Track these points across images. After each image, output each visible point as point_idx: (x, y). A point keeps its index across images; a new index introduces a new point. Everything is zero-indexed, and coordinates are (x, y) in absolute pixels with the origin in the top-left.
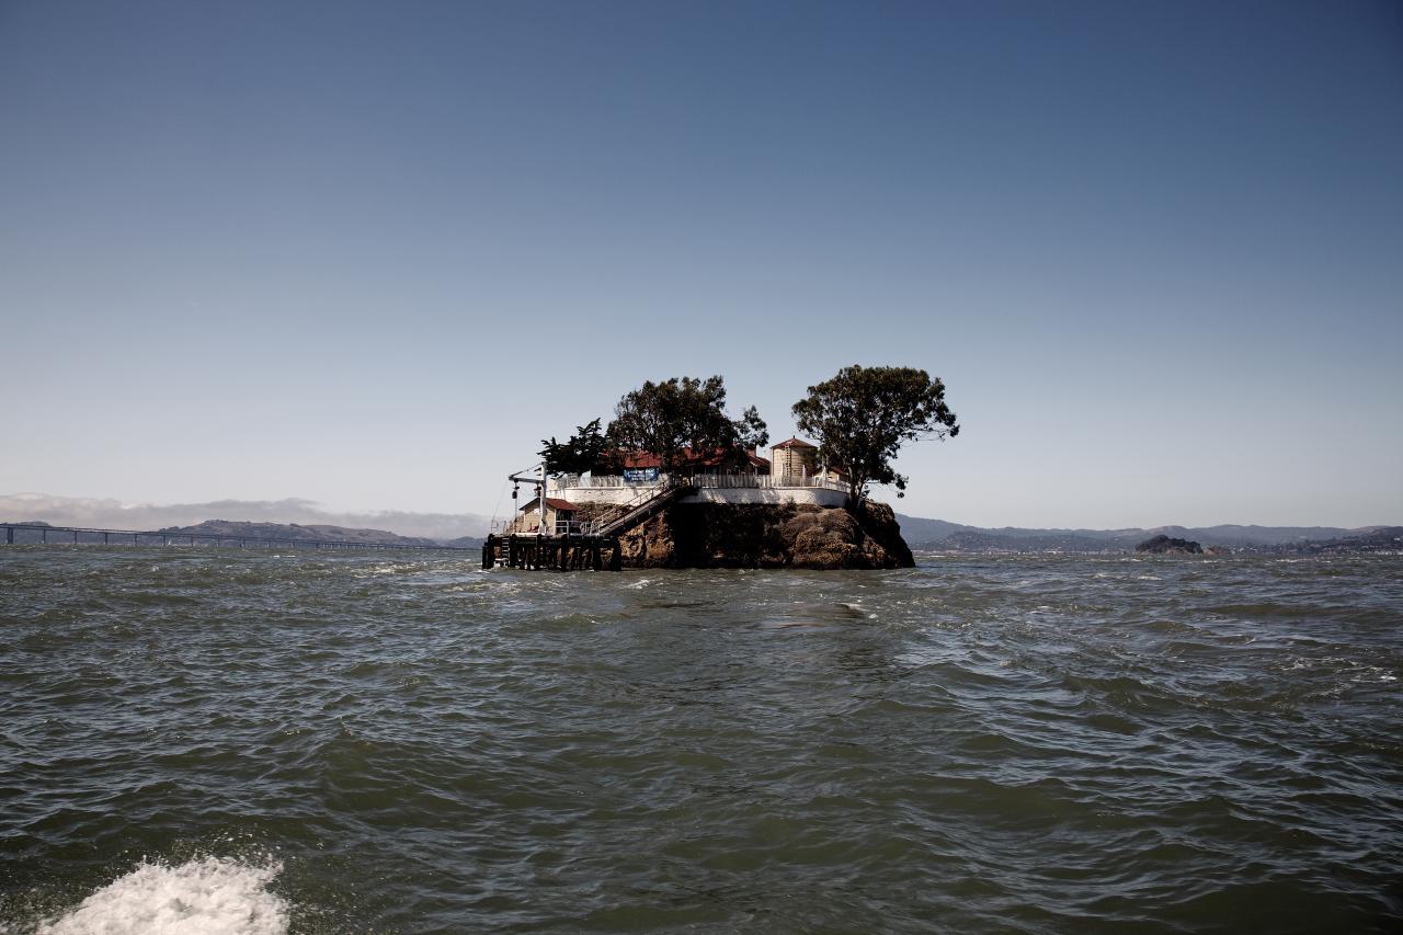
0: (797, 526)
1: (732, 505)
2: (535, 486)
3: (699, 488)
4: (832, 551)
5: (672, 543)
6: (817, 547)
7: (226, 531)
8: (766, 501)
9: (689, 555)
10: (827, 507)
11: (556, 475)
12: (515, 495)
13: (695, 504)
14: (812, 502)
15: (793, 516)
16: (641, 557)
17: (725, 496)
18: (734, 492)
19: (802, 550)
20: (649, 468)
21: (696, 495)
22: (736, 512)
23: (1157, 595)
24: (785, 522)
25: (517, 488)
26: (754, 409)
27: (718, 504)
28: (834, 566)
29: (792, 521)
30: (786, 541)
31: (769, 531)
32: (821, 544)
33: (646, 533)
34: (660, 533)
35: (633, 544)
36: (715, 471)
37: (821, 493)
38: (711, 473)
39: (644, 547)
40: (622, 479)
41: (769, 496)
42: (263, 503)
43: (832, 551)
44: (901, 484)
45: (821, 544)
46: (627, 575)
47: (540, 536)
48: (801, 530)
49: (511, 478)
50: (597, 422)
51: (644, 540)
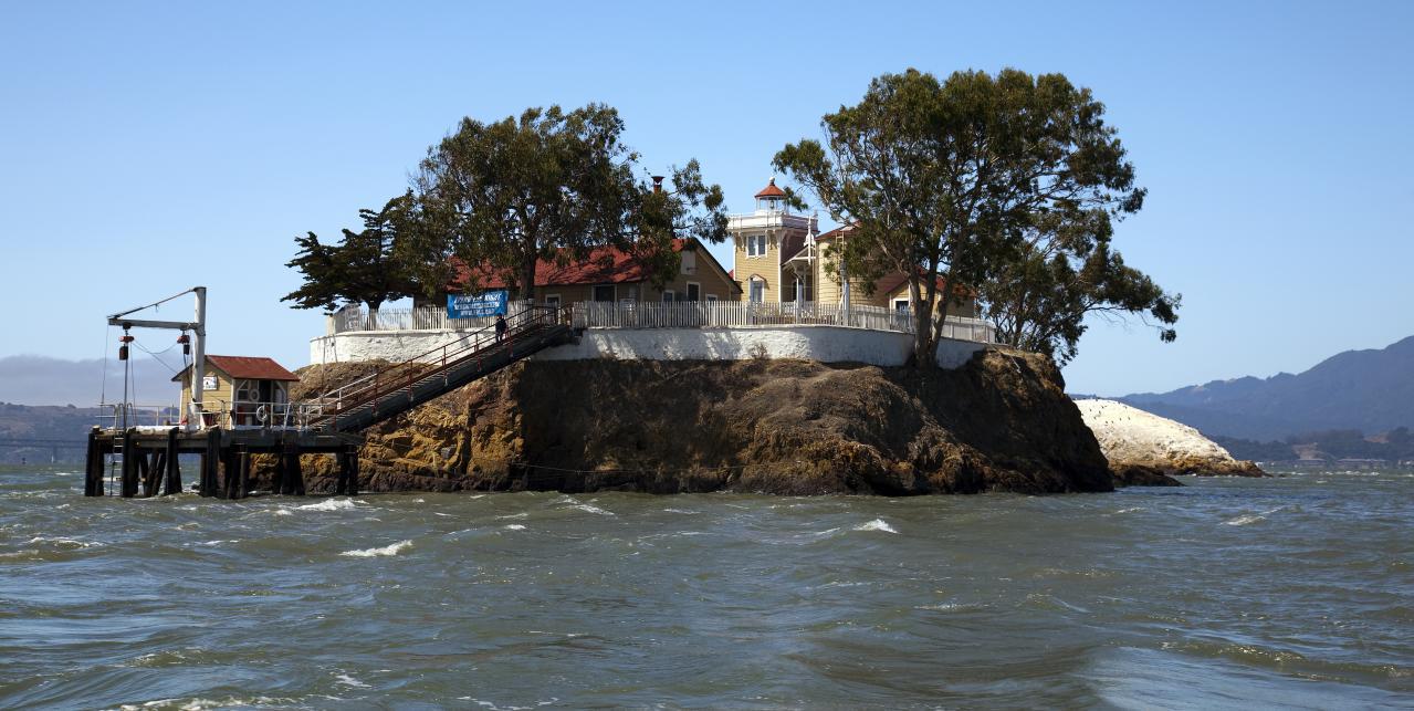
0: (759, 404)
1: (647, 362)
2: (178, 333)
3: (581, 330)
5: (518, 442)
6: (786, 446)
8: (714, 355)
9: (547, 465)
10: (834, 365)
11: (332, 307)
15: (755, 384)
17: (634, 346)
18: (650, 337)
22: (654, 377)
23: (290, 576)
24: (737, 397)
25: (128, 339)
26: (694, 166)
27: (619, 362)
28: (813, 488)
29: (750, 394)
31: (707, 416)
33: (472, 421)
34: (497, 421)
35: (445, 445)
36: (632, 292)
39: (466, 450)
40: (444, 314)
41: (719, 345)
42: (1191, 387)
43: (817, 457)
44: (1165, 312)
47: (176, 431)
48: (762, 414)
49: (114, 321)
51: (468, 435)
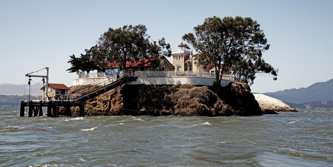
0: (179, 95)
2: (42, 78)
3: (137, 78)
4: (192, 107)
5: (122, 104)
6: (185, 105)
7: (5, 100)
8: (168, 83)
11: (78, 72)
12: (29, 83)
13: (135, 85)
14: (189, 83)
15: (178, 90)
16: (108, 111)
17: (149, 81)
19: (179, 107)
20: (116, 68)
21: (136, 80)
22: (154, 88)
25: (30, 80)
26: (163, 39)
27: (146, 85)
28: (192, 115)
29: (177, 92)
30: (173, 103)
31: (167, 98)
32: (187, 104)
33: (111, 99)
34: (117, 99)
35: (105, 105)
36: (149, 68)
37: (194, 77)
38: (147, 70)
39: (110, 106)
41: (169, 81)
42: (281, 91)
43: (192, 107)
44: (274, 73)
45: (187, 104)
46: (137, 117)
48: (180, 97)
49: (27, 75)
50: (190, 48)
51: (110, 102)
